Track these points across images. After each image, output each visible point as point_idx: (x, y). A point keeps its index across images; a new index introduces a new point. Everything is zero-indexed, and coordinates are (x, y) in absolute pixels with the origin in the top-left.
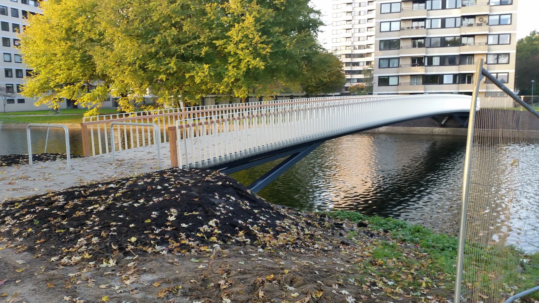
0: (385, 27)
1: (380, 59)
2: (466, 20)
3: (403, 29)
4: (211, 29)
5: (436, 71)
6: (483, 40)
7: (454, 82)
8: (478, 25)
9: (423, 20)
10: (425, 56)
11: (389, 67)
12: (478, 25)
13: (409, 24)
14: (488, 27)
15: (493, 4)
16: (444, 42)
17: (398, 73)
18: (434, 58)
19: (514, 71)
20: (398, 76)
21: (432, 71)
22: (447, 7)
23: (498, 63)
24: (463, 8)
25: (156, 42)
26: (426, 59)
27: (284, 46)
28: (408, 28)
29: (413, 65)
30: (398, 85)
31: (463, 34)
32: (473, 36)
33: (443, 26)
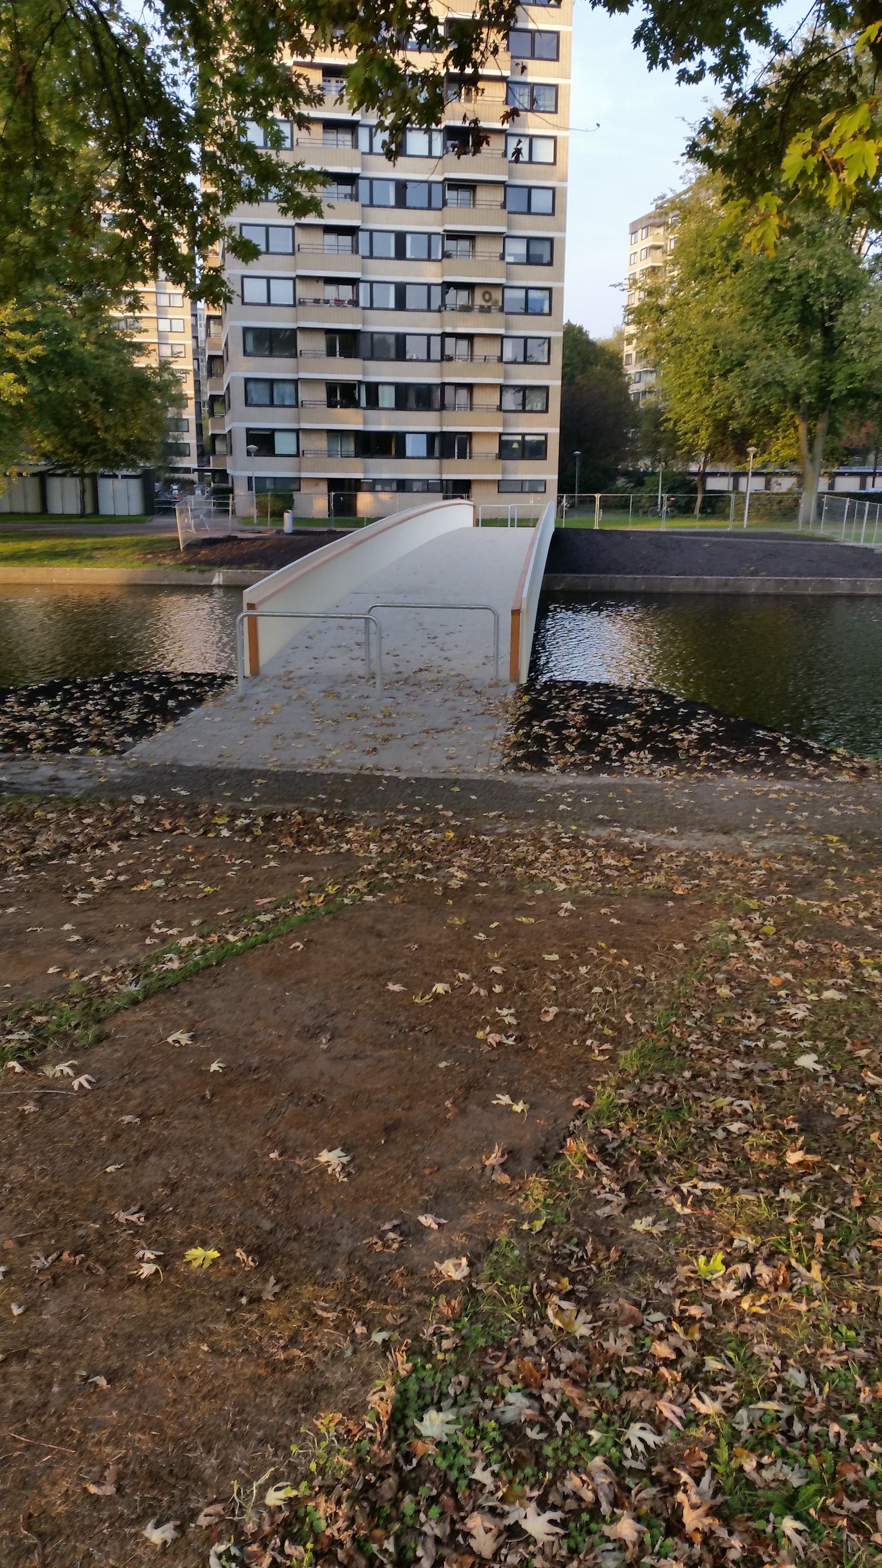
2: (452, 292)
3: (302, 303)
7: (430, 454)
9: (353, 282)
11: (272, 404)
14: (502, 316)
18: (380, 388)
19: (558, 430)
20: (297, 431)
23: (524, 411)
24: (445, 261)
28: (317, 301)
29: (331, 404)
30: (297, 455)
31: (449, 330)
32: (470, 337)
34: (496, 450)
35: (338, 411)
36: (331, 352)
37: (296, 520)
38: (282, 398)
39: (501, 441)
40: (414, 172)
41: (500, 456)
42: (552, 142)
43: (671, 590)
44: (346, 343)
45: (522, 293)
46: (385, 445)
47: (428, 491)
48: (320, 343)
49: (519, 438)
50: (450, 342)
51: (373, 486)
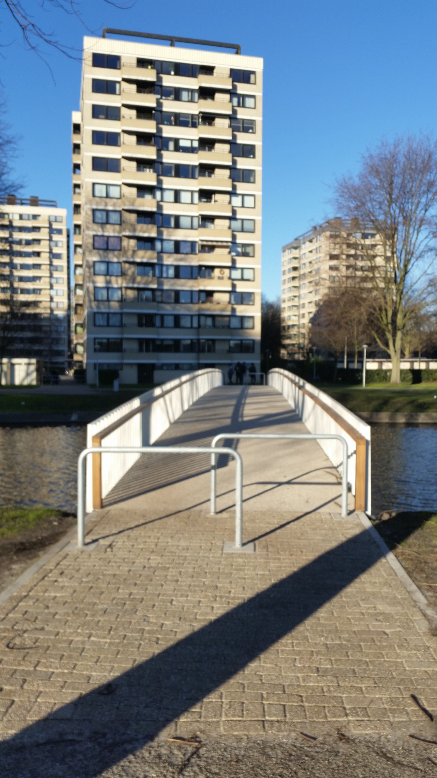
11: (108, 325)
35: (144, 329)
36: (141, 350)
37: (121, 386)
42: (253, 206)
48: (135, 346)
50: (202, 319)
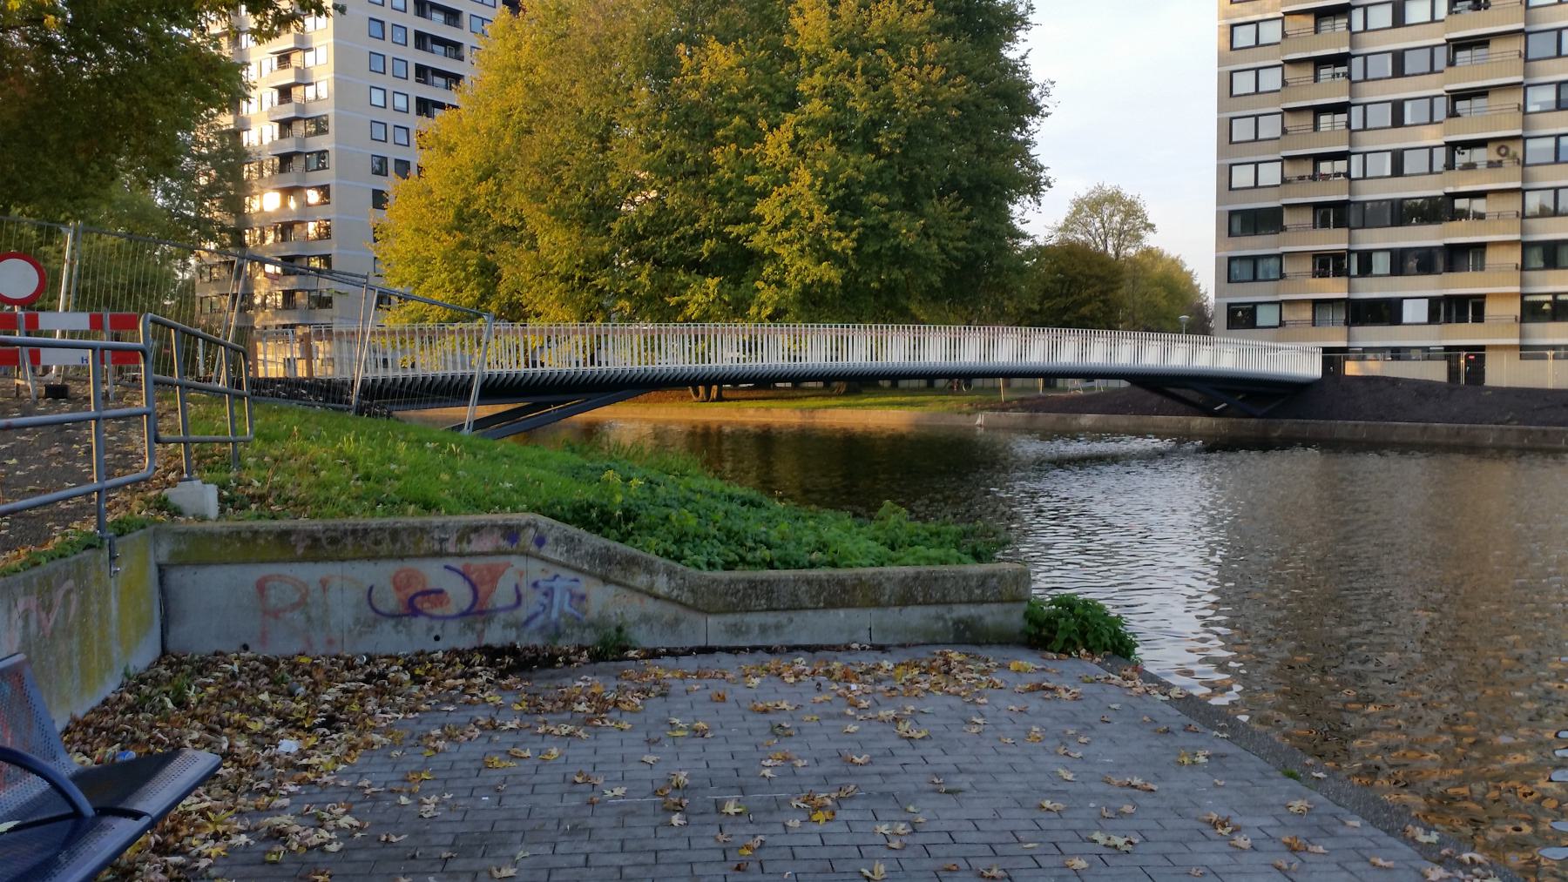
0: (1243, 177)
1: (1231, 259)
4: (723, 201)
5: (1381, 290)
6: (1514, 204)
7: (1433, 318)
8: (1491, 164)
10: (1350, 252)
11: (1255, 279)
12: (1491, 164)
13: (1307, 168)
15: (1537, 108)
16: (1402, 213)
17: (1277, 293)
18: (1374, 256)
20: (1280, 303)
21: (1371, 290)
22: (1408, 121)
25: (614, 234)
26: (1354, 259)
27: (896, 234)
28: (1301, 178)
33: (1398, 169)
34: (1518, 312)
38: (1266, 272)
39: (1523, 304)
40: (1413, 40)
41: (1523, 319)
43: (1395, 438)
44: (1335, 214)
45: (1552, 142)
46: (1388, 312)
47: (1429, 358)
49: (1550, 298)
51: (1363, 354)
